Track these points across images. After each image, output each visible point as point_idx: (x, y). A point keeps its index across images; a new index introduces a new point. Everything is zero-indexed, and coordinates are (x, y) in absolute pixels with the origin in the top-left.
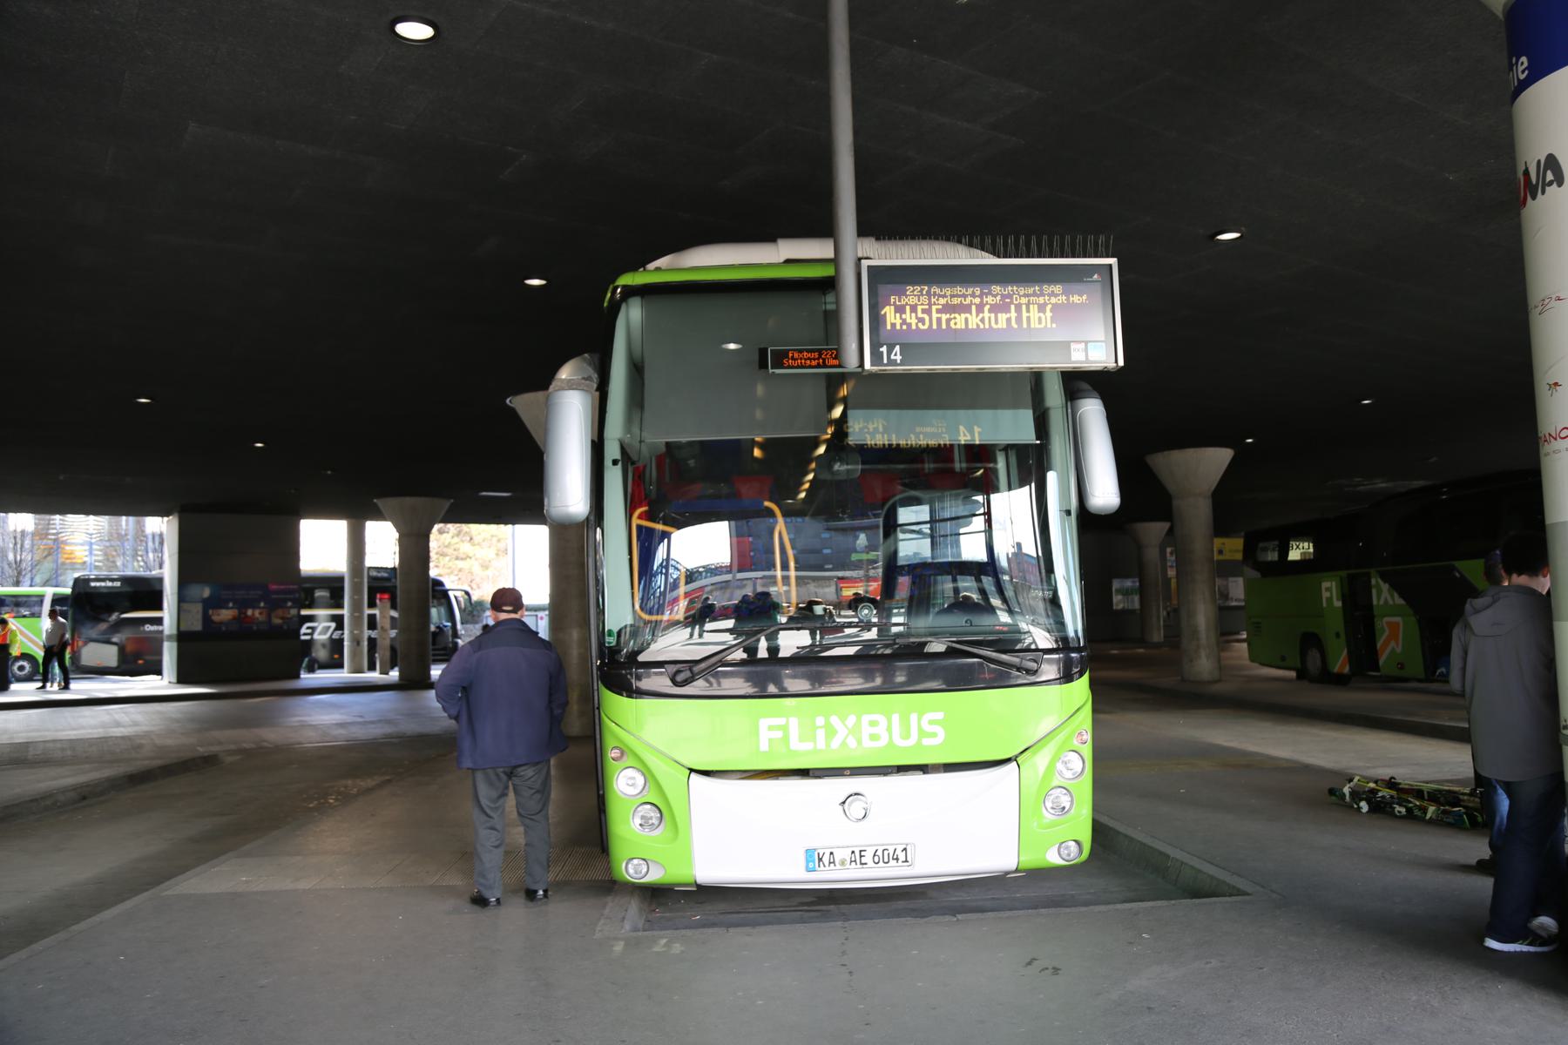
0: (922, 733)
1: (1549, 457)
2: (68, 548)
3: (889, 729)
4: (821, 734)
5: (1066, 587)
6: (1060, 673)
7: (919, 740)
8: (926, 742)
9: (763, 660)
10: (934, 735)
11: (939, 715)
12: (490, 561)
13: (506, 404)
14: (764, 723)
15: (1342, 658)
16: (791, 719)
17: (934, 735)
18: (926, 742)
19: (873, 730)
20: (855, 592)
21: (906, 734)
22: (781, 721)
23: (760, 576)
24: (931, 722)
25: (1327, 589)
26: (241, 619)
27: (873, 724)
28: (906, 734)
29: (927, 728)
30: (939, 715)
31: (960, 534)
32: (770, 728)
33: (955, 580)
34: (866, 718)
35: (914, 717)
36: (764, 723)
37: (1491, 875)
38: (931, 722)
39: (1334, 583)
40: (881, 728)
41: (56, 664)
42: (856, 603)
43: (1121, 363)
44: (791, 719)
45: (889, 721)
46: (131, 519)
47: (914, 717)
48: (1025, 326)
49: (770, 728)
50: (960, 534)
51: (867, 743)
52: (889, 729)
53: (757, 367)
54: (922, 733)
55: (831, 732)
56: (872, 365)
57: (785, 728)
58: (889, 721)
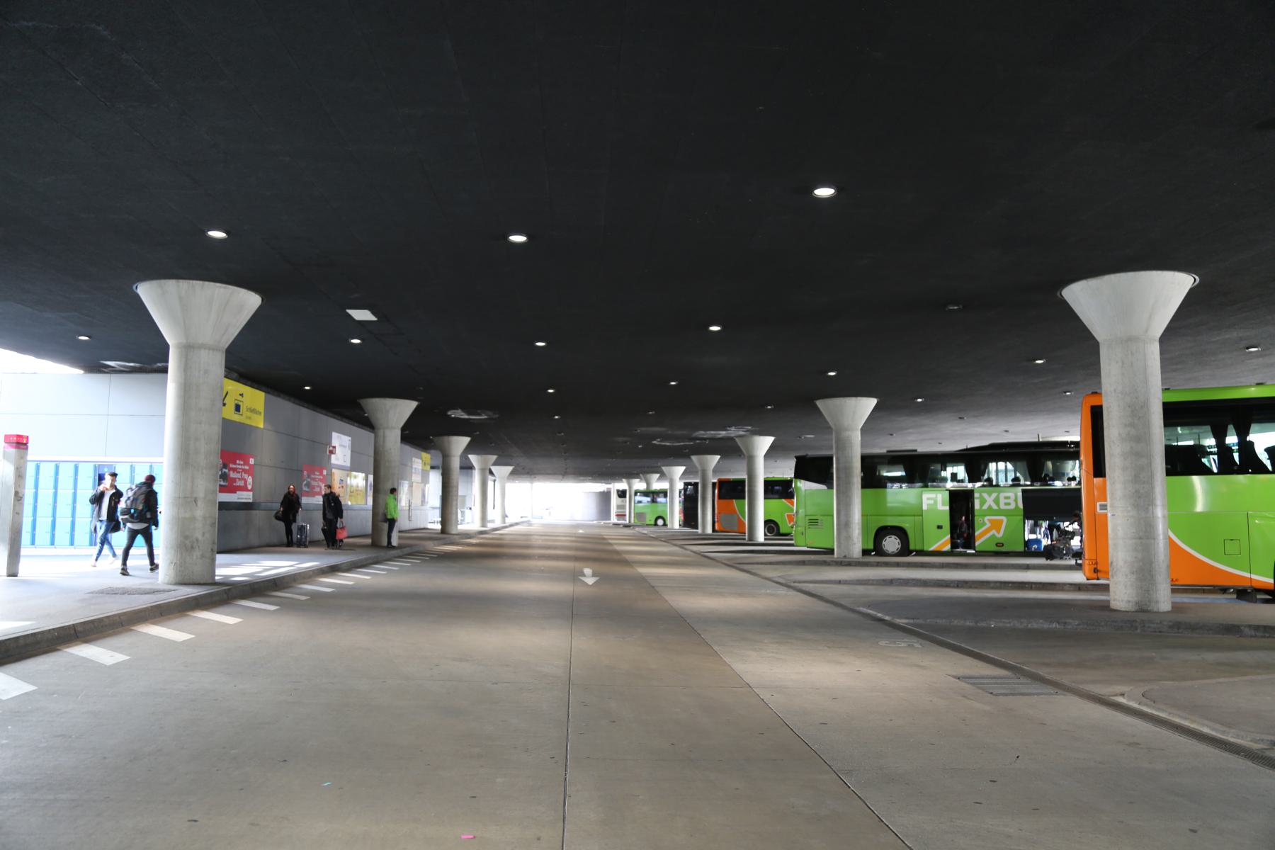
19: (1007, 501)
48: (1232, 440)
49: (928, 499)
55: (997, 501)
56: (162, 456)
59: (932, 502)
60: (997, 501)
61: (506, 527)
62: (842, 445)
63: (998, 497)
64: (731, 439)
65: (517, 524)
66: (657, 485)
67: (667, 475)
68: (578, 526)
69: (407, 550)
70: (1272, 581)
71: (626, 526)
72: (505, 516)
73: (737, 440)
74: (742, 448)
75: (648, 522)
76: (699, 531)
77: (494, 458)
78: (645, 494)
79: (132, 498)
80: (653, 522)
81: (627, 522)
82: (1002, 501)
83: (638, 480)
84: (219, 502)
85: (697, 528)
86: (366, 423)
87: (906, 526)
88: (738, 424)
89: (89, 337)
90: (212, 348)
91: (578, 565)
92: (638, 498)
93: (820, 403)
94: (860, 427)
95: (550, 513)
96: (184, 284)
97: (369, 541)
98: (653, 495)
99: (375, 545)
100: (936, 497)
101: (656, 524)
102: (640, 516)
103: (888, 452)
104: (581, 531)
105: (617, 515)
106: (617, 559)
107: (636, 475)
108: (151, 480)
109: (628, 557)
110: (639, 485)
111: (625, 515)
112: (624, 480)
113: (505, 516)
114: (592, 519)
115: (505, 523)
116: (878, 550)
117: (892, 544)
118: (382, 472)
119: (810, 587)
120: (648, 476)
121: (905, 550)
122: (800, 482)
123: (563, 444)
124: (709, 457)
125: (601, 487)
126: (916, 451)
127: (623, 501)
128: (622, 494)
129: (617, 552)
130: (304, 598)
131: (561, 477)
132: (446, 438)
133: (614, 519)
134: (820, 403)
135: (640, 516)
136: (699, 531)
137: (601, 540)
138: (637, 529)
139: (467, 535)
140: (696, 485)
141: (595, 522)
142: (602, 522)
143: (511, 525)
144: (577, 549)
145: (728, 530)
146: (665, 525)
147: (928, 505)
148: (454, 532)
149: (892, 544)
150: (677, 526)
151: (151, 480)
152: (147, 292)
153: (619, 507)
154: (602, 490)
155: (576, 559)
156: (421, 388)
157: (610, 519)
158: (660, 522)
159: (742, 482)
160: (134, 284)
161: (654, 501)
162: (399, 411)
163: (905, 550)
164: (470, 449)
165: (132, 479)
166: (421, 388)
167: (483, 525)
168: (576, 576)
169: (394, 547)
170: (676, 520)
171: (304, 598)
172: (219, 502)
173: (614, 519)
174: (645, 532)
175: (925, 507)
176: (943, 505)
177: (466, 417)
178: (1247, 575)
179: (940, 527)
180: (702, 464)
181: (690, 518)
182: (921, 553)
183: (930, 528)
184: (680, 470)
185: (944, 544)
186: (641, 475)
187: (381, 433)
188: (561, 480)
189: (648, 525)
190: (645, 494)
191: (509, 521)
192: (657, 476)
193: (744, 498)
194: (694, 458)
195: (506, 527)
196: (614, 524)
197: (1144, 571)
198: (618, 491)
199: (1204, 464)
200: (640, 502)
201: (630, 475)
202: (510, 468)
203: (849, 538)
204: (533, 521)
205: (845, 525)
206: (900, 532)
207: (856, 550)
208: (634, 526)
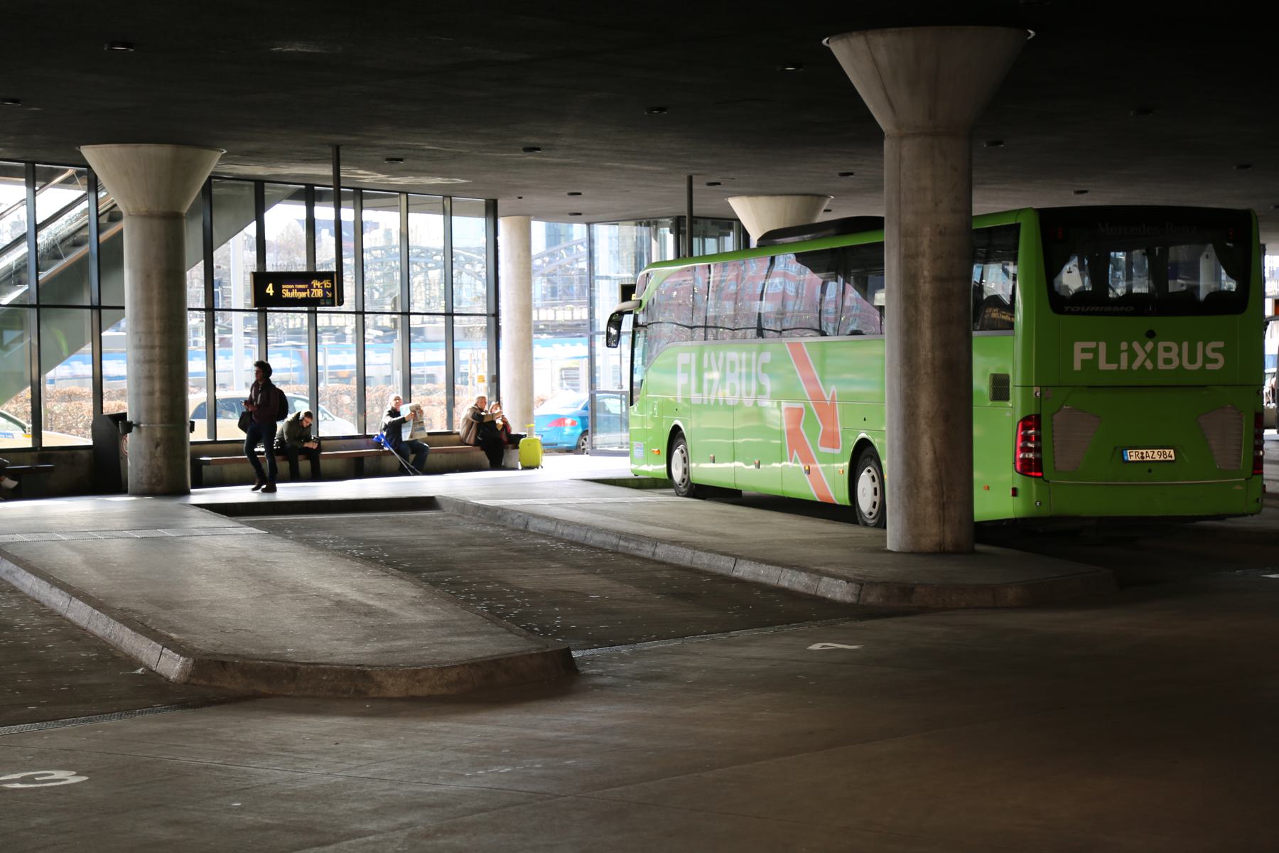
0: (1207, 360)
1: (143, 209)
2: (385, 691)
3: (1180, 355)
4: (1124, 358)
5: (333, 240)
7: (1204, 366)
8: (1209, 366)
9: (29, 286)
10: (1216, 361)
11: (1221, 344)
16: (1100, 343)
17: (1216, 361)
18: (1209, 366)
19: (1167, 355)
21: (1192, 360)
22: (1092, 345)
24: (1214, 350)
27: (1168, 350)
28: (1192, 360)
29: (1211, 355)
30: (1221, 344)
31: (444, 314)
32: (1084, 350)
33: (654, 553)
34: (1161, 345)
35: (1200, 345)
38: (1214, 350)
40: (1173, 355)
42: (316, 617)
43: (24, 180)
44: (1100, 343)
46: (266, 190)
47: (1200, 345)
49: (1084, 350)
50: (444, 314)
51: (1161, 366)
52: (1180, 355)
53: (621, 300)
54: (1207, 360)
55: (1133, 356)
57: (1095, 351)
59: (1089, 356)
60: (1153, 356)
63: (1155, 349)
79: (575, 722)
82: (1162, 355)
84: (883, 288)
100: (1098, 346)
108: (300, 413)
111: (123, 308)
122: (1230, 288)
130: (225, 329)
151: (300, 413)
156: (367, 706)
165: (286, 383)
166: (367, 706)
171: (225, 329)
172: (883, 288)
199: (1231, 274)
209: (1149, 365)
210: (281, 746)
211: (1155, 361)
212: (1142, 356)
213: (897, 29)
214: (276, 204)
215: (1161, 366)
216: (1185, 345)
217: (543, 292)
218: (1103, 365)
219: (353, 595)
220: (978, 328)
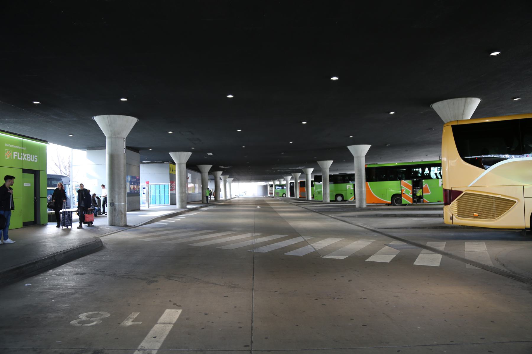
6: (173, 203)
7: (34, 161)
9: (23, 185)
10: (36, 160)
11: (37, 156)
12: (443, 189)
13: (37, 162)
14: (347, 186)
15: (408, 201)
20: (207, 173)
21: (33, 159)
22: (349, 185)
23: (498, 195)
24: (36, 157)
25: (15, 154)
26: (417, 180)
29: (36, 159)
30: (37, 156)
32: (348, 186)
35: (34, 156)
36: (347, 186)
37: (191, 173)
38: (36, 157)
39: (351, 185)
40: (29, 157)
41: (139, 313)
45: (31, 156)
49: (348, 186)
57: (350, 187)
58: (31, 156)
59: (349, 187)
61: (232, 199)
62: (324, 173)
64: (301, 169)
65: (235, 198)
66: (283, 182)
67: (305, 173)
68: (256, 198)
69: (212, 204)
70: (390, 202)
71: (273, 197)
72: (231, 195)
73: (303, 170)
74: (304, 171)
75: (280, 196)
76: (295, 198)
77: (228, 176)
78: (279, 186)
80: (282, 195)
81: (274, 196)
82: (28, 157)
83: (277, 181)
84: (105, 148)
85: (294, 196)
86: (199, 171)
87: (343, 194)
88: (302, 166)
89: (73, 135)
90: (184, 164)
91: (256, 206)
92: (277, 187)
93: (318, 162)
94: (299, 176)
95: (245, 194)
96: (180, 152)
97: (201, 202)
98: (283, 186)
99: (203, 203)
101: (283, 196)
102: (277, 193)
103: (339, 174)
104: (257, 199)
105: (270, 194)
106: (267, 204)
107: (276, 179)
109: (269, 204)
110: (277, 183)
111: (273, 193)
112: (272, 181)
113: (231, 195)
114: (260, 195)
115: (231, 197)
116: (336, 200)
117: (339, 198)
118: (204, 184)
119: (306, 208)
120: (280, 179)
121: (343, 200)
123: (249, 169)
124: (297, 174)
125: (263, 184)
126: (346, 173)
127: (272, 189)
128: (271, 186)
129: (267, 203)
131: (249, 181)
132: (215, 172)
133: (269, 195)
134: (318, 162)
135: (277, 193)
136: (295, 198)
137: (263, 201)
138: (276, 198)
139: (222, 201)
140: (293, 183)
141: (262, 196)
142: (265, 196)
143: (233, 198)
144: (256, 203)
145: (318, 199)
146: (286, 196)
147: (348, 188)
148: (219, 200)
149: (339, 198)
150: (289, 197)
152: (98, 119)
153: (270, 191)
154: (263, 185)
155: (256, 205)
157: (267, 195)
158: (284, 195)
159: (304, 182)
160: (93, 117)
161: (283, 188)
162: (207, 168)
163: (343, 200)
164: (222, 175)
167: (226, 198)
168: (256, 207)
169: (208, 203)
170: (289, 196)
172: (103, 147)
173: (269, 195)
174: (278, 199)
175: (347, 189)
176: (352, 188)
177: (224, 167)
178: (386, 201)
179: (351, 194)
180: (295, 176)
181: (292, 194)
182: (346, 201)
183: (349, 195)
184: (311, 170)
185: (352, 198)
186: (277, 179)
187: (203, 173)
188: (249, 182)
189: (280, 197)
190: (279, 186)
191: (232, 197)
192: (283, 179)
193: (305, 187)
194: (292, 174)
195: (232, 199)
196: (269, 197)
197: (361, 201)
198: (270, 185)
200: (278, 189)
201: (274, 179)
202: (232, 179)
203: (326, 197)
204: (240, 197)
205: (325, 194)
206: (342, 195)
207: (328, 200)
208: (275, 197)
209: (26, 159)
210: (60, 275)
211: (27, 158)
212: (25, 157)
213: (460, 123)
214: (302, 256)
215: (28, 160)
216: (31, 155)
217: (306, 163)
218: (19, 158)
219: (198, 243)
220: (197, 168)
